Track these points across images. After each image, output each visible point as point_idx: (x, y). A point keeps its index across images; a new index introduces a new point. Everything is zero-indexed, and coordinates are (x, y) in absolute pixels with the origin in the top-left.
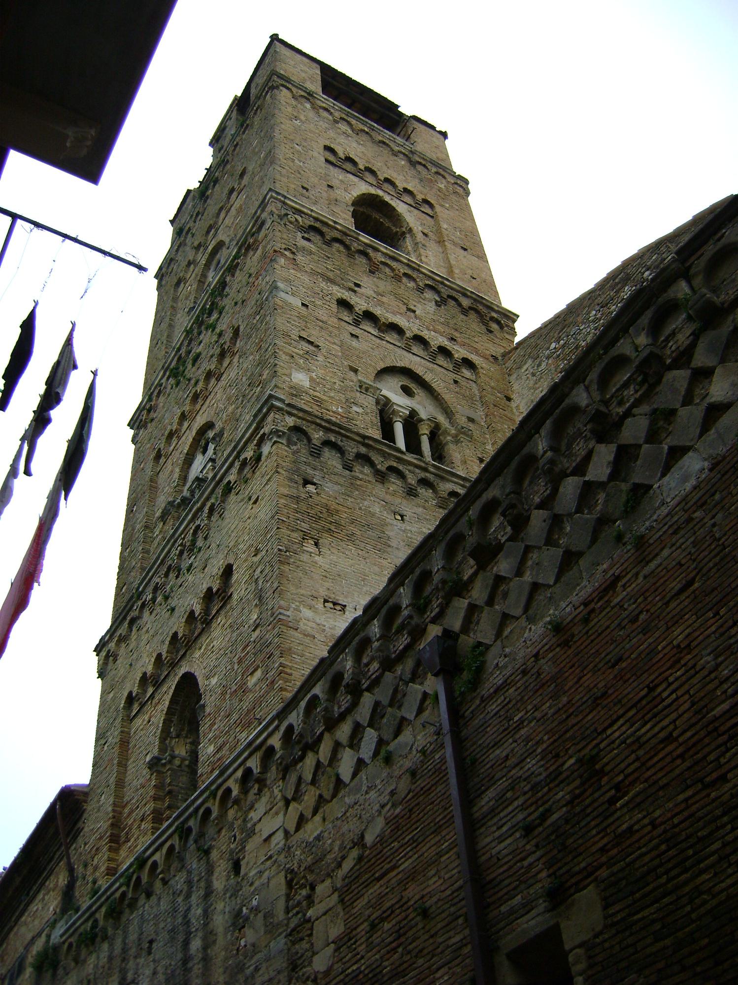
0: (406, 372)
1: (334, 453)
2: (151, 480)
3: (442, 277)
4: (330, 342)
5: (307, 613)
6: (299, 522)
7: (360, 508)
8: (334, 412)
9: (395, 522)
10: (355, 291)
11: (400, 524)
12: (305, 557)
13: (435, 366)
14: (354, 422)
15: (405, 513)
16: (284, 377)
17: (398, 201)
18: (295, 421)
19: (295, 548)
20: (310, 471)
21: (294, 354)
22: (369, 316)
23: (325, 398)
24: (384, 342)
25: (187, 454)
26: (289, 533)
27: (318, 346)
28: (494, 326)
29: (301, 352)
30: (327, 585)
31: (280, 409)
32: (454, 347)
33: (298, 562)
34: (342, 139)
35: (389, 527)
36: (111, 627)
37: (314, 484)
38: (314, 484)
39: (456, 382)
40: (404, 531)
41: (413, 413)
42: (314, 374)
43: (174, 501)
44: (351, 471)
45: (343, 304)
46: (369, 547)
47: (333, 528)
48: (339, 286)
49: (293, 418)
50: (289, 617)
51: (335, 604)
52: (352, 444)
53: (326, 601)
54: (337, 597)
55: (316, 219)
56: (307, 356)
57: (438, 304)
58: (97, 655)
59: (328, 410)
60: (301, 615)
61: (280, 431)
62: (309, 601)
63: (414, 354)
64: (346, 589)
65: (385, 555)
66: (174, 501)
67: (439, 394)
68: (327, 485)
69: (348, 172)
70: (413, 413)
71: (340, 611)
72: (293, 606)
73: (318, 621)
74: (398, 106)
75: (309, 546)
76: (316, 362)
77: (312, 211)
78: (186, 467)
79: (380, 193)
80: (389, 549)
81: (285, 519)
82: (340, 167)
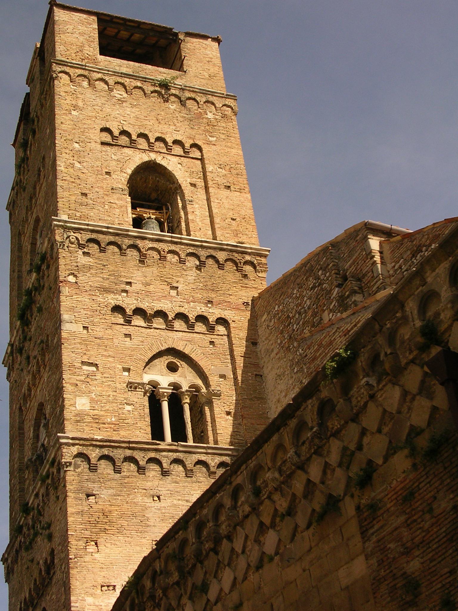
0: (172, 351)
1: (108, 463)
2: (19, 429)
3: (202, 241)
4: (105, 356)
5: (90, 600)
6: (83, 531)
7: (127, 503)
8: (109, 424)
9: (153, 504)
10: (126, 291)
11: (157, 504)
12: (88, 558)
13: (195, 335)
14: (126, 421)
15: (161, 493)
16: (70, 408)
17: (169, 157)
18: (78, 448)
19: (80, 554)
20: (90, 485)
21: (78, 382)
22: (139, 312)
23: (102, 413)
24: (152, 330)
25: (36, 420)
26: (77, 543)
27: (96, 365)
28: (248, 269)
29: (82, 378)
30: (103, 574)
31: (67, 444)
32: (211, 311)
33: (84, 563)
34: (116, 112)
35: (149, 509)
36: (10, 542)
37: (94, 495)
38: (94, 495)
39: (212, 343)
40: (159, 509)
41: (176, 386)
42: (93, 394)
43: (32, 459)
44: (120, 473)
45: (118, 309)
46: (133, 533)
47: (107, 527)
48: (113, 292)
49: (77, 446)
50: (77, 607)
51: (108, 586)
52: (120, 451)
53: (102, 586)
54: (110, 581)
55: (92, 231)
56: (88, 380)
57: (198, 268)
58: (3, 564)
59: (104, 424)
60: (86, 603)
61: (67, 462)
62: (91, 591)
63: (176, 331)
64: (116, 572)
65: (146, 535)
66: (32, 459)
67: (196, 362)
68: (103, 492)
69: (124, 147)
70: (176, 386)
71: (112, 590)
72: (80, 598)
73: (97, 603)
74: (171, 29)
75: (92, 548)
76: (95, 382)
77: (88, 225)
78: (36, 428)
79: (153, 156)
80: (149, 528)
81: (73, 533)
82: (116, 145)
